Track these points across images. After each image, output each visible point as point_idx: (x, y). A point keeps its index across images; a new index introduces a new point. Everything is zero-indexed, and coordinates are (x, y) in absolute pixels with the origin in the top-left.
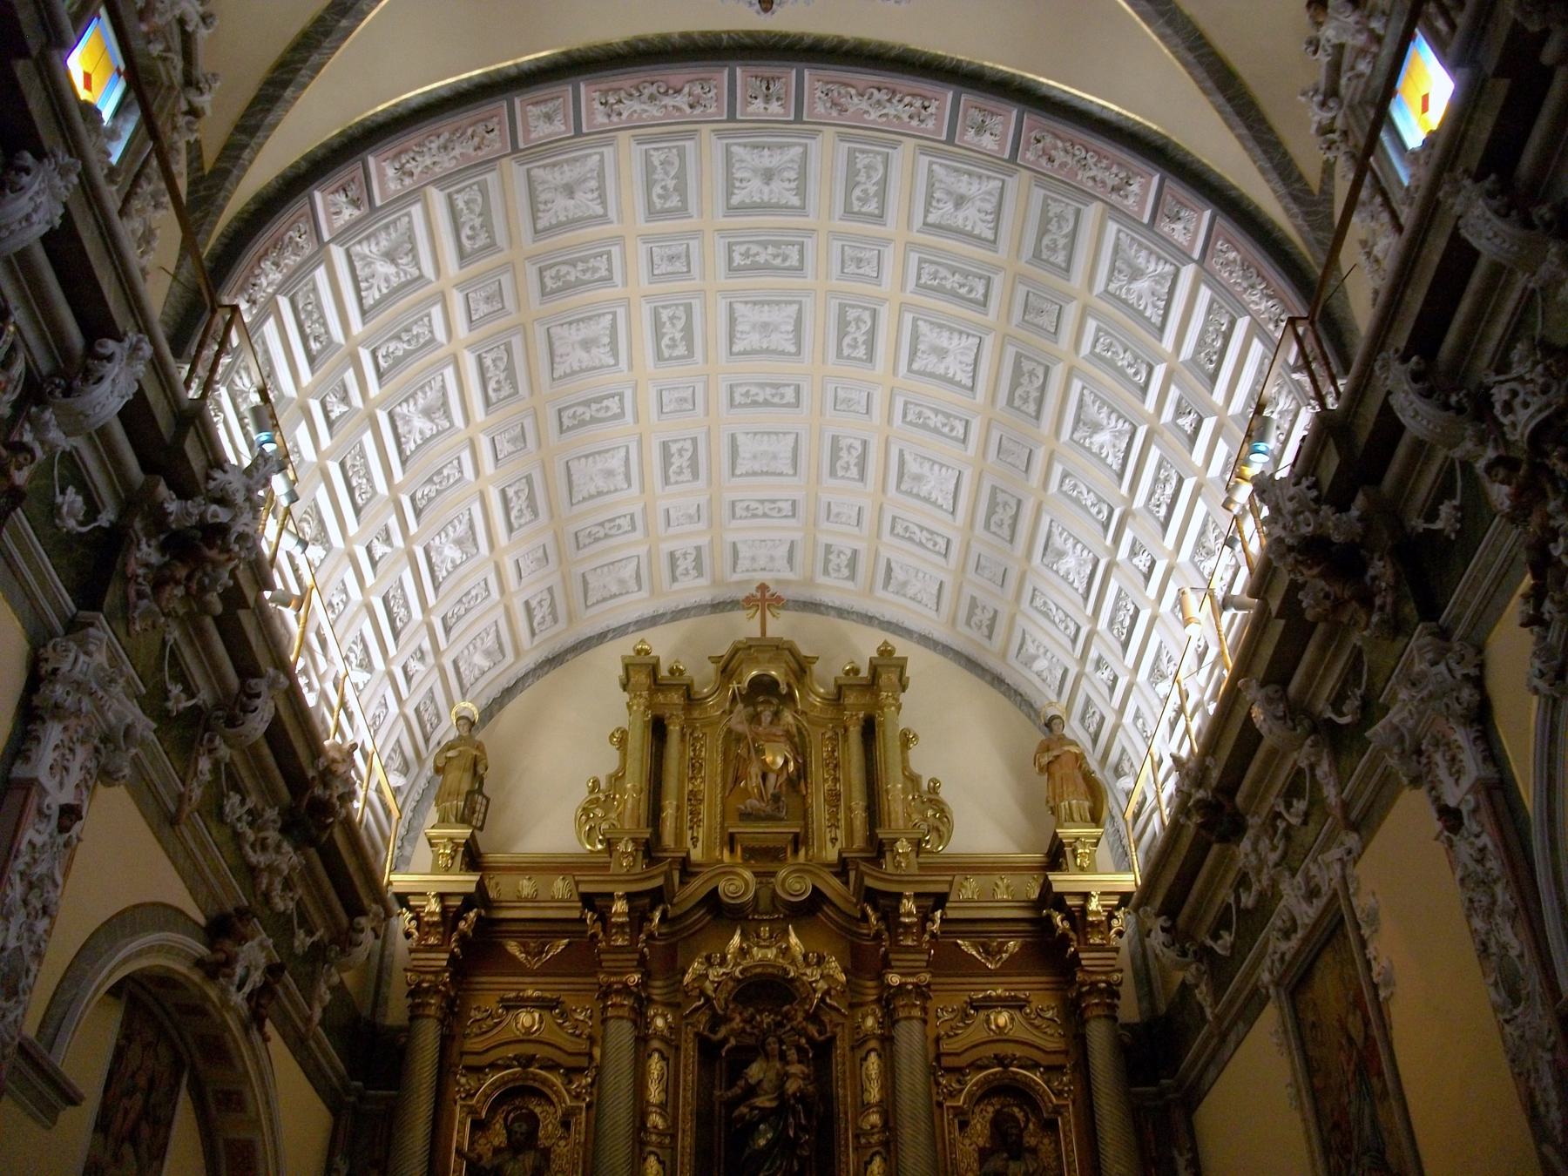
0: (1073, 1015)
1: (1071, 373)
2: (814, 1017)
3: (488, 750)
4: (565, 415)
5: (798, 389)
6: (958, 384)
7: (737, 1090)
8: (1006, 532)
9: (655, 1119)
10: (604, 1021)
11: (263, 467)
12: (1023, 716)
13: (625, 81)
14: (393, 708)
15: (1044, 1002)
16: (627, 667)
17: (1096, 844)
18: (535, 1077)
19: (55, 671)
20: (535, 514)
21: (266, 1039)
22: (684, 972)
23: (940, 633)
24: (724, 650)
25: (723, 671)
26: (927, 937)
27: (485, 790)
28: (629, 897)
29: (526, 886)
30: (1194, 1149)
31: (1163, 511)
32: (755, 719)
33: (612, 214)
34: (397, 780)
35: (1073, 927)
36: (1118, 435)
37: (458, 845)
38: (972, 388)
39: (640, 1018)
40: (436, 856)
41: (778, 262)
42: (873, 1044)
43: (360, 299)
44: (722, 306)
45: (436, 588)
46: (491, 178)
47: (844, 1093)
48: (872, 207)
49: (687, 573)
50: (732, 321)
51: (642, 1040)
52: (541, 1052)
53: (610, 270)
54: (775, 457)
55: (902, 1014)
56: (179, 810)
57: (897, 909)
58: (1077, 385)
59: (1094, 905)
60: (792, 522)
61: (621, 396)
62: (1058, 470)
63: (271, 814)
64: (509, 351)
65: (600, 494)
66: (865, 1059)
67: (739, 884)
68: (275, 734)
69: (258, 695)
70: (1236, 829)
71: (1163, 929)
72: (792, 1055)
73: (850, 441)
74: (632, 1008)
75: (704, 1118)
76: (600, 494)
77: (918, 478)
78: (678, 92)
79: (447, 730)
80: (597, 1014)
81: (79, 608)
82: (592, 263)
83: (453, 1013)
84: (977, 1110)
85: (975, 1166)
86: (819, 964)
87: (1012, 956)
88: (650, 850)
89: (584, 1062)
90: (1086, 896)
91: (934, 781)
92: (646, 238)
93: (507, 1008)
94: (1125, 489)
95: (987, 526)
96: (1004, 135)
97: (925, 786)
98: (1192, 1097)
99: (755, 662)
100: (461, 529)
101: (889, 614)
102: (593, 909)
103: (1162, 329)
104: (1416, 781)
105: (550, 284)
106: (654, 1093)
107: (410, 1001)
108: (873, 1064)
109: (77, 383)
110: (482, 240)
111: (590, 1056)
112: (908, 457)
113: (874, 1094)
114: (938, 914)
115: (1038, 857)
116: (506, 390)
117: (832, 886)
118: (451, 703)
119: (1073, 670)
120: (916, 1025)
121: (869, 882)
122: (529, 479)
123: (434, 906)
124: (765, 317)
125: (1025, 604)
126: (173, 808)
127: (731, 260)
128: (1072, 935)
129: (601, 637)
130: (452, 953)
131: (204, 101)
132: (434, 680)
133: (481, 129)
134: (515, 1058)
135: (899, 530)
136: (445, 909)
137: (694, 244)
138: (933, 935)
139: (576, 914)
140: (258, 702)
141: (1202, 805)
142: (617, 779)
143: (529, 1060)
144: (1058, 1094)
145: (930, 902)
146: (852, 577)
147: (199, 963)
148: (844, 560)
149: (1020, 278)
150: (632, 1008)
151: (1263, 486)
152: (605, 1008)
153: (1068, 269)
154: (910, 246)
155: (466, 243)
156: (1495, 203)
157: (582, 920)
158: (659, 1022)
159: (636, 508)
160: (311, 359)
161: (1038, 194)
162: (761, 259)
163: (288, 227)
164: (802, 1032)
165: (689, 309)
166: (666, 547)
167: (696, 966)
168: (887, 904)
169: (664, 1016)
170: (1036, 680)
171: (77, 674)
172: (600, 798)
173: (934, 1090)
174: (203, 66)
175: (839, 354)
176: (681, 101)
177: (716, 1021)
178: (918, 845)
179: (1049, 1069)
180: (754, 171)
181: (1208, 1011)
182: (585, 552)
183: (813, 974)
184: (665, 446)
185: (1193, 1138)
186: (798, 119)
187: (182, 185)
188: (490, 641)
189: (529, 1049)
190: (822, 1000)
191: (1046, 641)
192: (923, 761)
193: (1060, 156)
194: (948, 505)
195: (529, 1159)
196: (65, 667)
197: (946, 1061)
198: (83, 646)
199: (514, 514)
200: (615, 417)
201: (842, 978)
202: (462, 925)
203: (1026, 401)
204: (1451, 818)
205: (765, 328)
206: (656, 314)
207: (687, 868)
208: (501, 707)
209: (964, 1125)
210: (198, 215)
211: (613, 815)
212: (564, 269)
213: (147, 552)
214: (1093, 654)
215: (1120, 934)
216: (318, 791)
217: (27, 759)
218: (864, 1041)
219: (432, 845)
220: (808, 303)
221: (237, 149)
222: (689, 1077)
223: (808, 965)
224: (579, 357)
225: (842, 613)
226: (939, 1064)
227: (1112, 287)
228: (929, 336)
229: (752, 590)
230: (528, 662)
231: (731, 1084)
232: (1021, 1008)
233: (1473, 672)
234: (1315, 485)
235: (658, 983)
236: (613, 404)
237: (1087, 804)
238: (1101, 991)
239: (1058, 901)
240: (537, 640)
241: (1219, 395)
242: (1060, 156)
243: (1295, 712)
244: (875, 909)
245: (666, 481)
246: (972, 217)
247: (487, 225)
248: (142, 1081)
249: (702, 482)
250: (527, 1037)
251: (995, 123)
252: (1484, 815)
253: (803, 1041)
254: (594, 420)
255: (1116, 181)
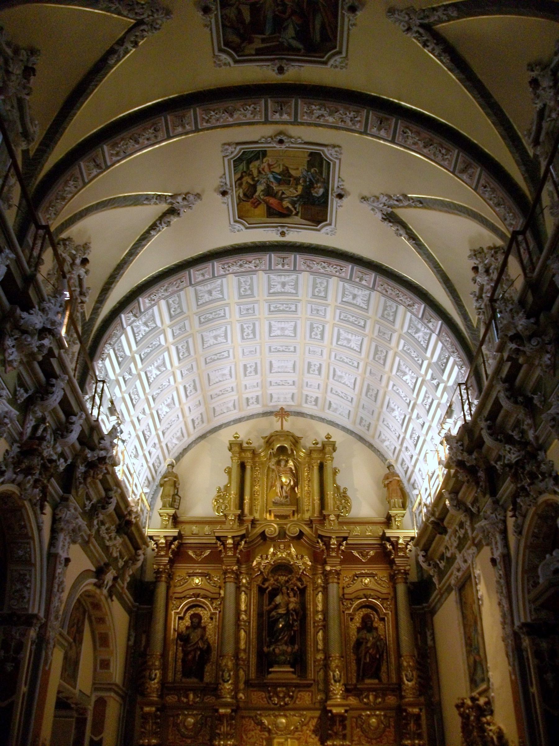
0: (392, 578)
1: (396, 354)
2: (300, 580)
3: (180, 478)
4: (202, 318)
5: (295, 347)
6: (355, 350)
7: (271, 606)
8: (373, 398)
9: (243, 616)
10: (225, 583)
11: (114, 432)
12: (380, 460)
13: (231, 260)
14: (145, 466)
15: (382, 573)
16: (230, 444)
17: (403, 517)
18: (200, 601)
19: (61, 518)
20: (196, 390)
21: (112, 601)
22: (253, 562)
23: (350, 426)
24: (267, 434)
25: (267, 442)
26: (340, 552)
27: (179, 494)
28: (233, 537)
29: (195, 529)
30: (433, 629)
31: (427, 407)
32: (278, 463)
33: (226, 297)
34: (146, 490)
35: (394, 548)
36: (425, 334)
37: (170, 516)
38: (360, 352)
39: (237, 580)
40: (163, 520)
41: (287, 309)
42: (320, 589)
43: (135, 339)
44: (267, 323)
45: (160, 421)
46: (182, 293)
47: (310, 607)
48: (322, 294)
49: (253, 403)
50: (270, 327)
51: (238, 589)
52: (202, 592)
53: (225, 314)
54: (286, 367)
55: (330, 581)
56: (89, 539)
57: (329, 542)
58: (397, 359)
59: (401, 541)
60: (293, 387)
61: (228, 351)
62: (391, 383)
63: (113, 528)
64: (187, 342)
65: (220, 381)
66: (317, 594)
67: (273, 529)
68: (117, 509)
69: (111, 498)
70: (444, 531)
71: (423, 556)
72: (291, 594)
73: (317, 325)
74: (234, 578)
75: (260, 615)
76: (220, 381)
77: (341, 377)
78: (250, 262)
79: (163, 468)
80: (222, 579)
81: (64, 492)
82: (218, 312)
83: (170, 577)
84: (357, 613)
85: (356, 634)
86: (301, 559)
87: (372, 557)
88: (241, 518)
89: (217, 596)
90: (398, 538)
91: (345, 488)
92: (238, 304)
93: (189, 576)
94: (415, 395)
95: (366, 395)
96: (370, 281)
97: (342, 491)
98: (433, 612)
99: (279, 441)
100: (169, 401)
101: (330, 418)
102: (220, 540)
103: (426, 349)
104: (488, 545)
105: (202, 320)
106: (243, 607)
107: (155, 575)
108: (320, 596)
109: (65, 433)
110: (179, 311)
111: (220, 594)
112: (337, 370)
113: (320, 608)
114: (345, 542)
115: (383, 519)
116: (186, 354)
117: (306, 530)
118: (165, 459)
119: (398, 448)
120: (335, 585)
121: (320, 532)
122: (194, 381)
123: (163, 541)
124: (283, 326)
125: (381, 423)
126: (87, 539)
127: (270, 309)
128: (393, 551)
129: (220, 427)
130: (170, 558)
131: (86, 299)
132: (159, 452)
133: (179, 281)
134: (193, 594)
135: (334, 392)
136: (167, 541)
137: (256, 305)
138: (343, 551)
139: (214, 541)
140: (112, 500)
141: (433, 522)
142: (227, 488)
143: (198, 595)
144: (386, 609)
145: (341, 539)
146: (316, 404)
147: (95, 584)
148: (313, 399)
149: (377, 322)
150: (234, 578)
151: (448, 438)
152: (225, 578)
153: (394, 322)
154: (337, 307)
155: (172, 313)
156: (507, 394)
157: (216, 543)
158: (244, 581)
159: (234, 385)
160: (119, 363)
161: (383, 299)
162: (281, 308)
163: (113, 329)
164: (295, 585)
165: (254, 325)
166: (245, 396)
167: (258, 559)
168: (326, 540)
169: (246, 579)
170: (386, 449)
171: (66, 518)
172: (222, 495)
173: (342, 606)
174: (86, 284)
175: (311, 337)
176: (252, 266)
177: (265, 580)
178: (338, 516)
179: (383, 599)
180: (279, 282)
181: (437, 586)
182: (213, 401)
183: (300, 563)
184: (245, 366)
185: (433, 625)
186: (295, 269)
187: (80, 329)
188: (179, 434)
189: (198, 591)
190: (303, 573)
191: (388, 436)
192: (342, 481)
193: (390, 291)
194: (352, 386)
195: (199, 631)
196: (64, 516)
197: (346, 596)
198: (68, 507)
199: (188, 392)
200: (226, 357)
201: (309, 563)
202: (173, 546)
203: (380, 359)
204: (493, 561)
205: (282, 329)
206: (242, 326)
207: (254, 522)
208: (183, 456)
209: (352, 619)
210: (85, 336)
211: (226, 502)
212: (208, 315)
213: (82, 468)
214: (405, 445)
215: (410, 551)
216: (128, 518)
217: (54, 547)
218: (317, 588)
219: (161, 516)
220: (299, 322)
221: (96, 311)
222: (254, 601)
223: (297, 559)
224: (212, 341)
225: (312, 417)
226: (342, 598)
227: (409, 331)
228: (344, 335)
229: (278, 409)
230: (193, 438)
231: (270, 603)
232: (374, 577)
233: (503, 518)
234: (462, 445)
235: (244, 566)
236: (226, 354)
237: (401, 500)
238: (402, 573)
239: (388, 539)
240: (196, 430)
241: (445, 377)
242: (390, 291)
243: (459, 504)
244: (322, 541)
245: (245, 375)
246: (359, 301)
247: (180, 306)
248: (76, 621)
249: (258, 376)
250: (197, 587)
251: (367, 277)
252: (502, 563)
253: (295, 588)
254: (218, 359)
255: (410, 303)
